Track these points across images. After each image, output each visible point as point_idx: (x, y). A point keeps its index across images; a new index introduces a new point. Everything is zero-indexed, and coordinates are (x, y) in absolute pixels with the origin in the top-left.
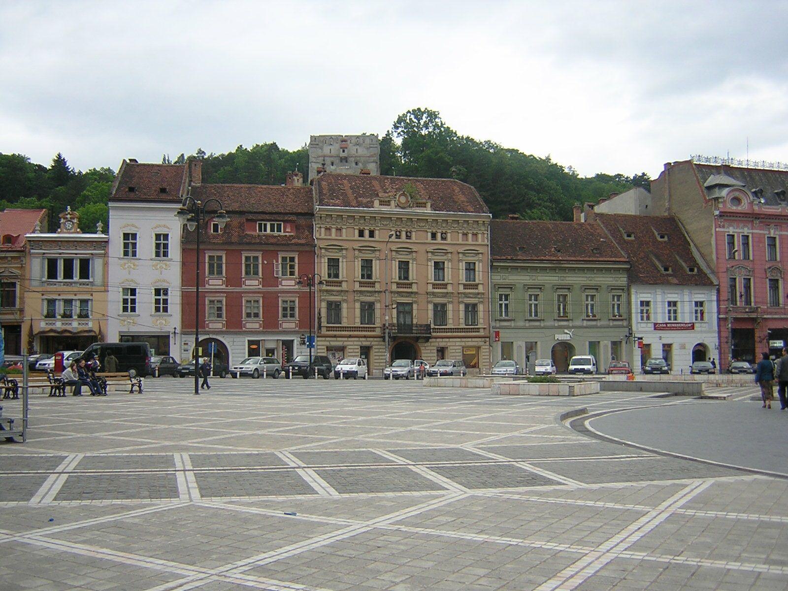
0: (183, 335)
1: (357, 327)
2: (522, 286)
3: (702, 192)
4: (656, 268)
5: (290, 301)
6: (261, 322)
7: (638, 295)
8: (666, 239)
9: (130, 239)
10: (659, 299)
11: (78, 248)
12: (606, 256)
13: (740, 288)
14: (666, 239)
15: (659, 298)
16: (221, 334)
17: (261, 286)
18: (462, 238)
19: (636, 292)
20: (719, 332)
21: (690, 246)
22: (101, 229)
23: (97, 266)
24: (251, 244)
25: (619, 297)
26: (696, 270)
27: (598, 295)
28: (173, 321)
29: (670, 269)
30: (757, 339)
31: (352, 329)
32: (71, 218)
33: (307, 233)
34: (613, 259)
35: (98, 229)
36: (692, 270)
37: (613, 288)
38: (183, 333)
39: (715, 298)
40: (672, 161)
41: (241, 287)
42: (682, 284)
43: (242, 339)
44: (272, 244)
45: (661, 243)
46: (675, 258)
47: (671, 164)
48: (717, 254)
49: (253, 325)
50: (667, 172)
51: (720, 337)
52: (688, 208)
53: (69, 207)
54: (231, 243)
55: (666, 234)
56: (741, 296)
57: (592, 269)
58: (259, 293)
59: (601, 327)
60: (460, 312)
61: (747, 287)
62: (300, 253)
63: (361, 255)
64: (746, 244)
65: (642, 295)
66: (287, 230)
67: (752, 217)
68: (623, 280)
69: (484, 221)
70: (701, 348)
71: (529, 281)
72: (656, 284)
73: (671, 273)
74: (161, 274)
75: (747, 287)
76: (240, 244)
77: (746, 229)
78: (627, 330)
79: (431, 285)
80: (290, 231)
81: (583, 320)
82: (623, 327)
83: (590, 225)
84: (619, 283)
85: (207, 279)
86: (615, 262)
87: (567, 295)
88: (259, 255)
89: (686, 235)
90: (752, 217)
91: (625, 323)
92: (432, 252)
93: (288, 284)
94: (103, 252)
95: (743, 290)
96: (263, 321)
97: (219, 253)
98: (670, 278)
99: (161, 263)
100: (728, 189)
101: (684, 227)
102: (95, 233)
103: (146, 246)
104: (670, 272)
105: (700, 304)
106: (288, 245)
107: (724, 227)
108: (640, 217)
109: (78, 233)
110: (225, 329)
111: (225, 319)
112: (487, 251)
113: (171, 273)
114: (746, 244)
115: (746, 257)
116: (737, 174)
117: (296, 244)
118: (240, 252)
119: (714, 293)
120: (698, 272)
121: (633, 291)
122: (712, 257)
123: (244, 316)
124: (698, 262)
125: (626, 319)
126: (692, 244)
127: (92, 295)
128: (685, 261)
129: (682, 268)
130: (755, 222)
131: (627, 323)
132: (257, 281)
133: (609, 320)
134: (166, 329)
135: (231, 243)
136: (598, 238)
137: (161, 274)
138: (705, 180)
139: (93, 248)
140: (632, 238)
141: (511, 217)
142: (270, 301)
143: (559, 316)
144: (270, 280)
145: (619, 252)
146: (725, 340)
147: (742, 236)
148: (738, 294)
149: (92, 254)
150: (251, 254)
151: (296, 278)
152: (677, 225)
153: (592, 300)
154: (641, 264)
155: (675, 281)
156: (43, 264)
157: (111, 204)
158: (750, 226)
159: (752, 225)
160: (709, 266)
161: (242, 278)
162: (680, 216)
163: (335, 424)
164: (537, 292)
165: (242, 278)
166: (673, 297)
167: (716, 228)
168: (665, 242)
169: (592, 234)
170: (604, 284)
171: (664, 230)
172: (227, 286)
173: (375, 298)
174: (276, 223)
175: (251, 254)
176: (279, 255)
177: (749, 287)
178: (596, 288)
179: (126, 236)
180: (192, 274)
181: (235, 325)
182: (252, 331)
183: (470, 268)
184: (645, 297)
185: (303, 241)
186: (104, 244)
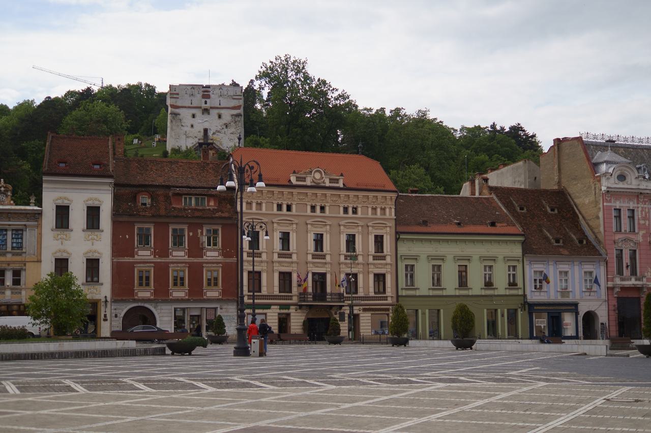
0: (113, 304)
1: (276, 296)
2: (426, 256)
5: (146, 271)
6: (187, 291)
8: (556, 211)
9: (63, 213)
11: (11, 219)
13: (626, 260)
15: (576, 268)
16: (150, 302)
17: (186, 257)
18: (246, 206)
21: (579, 218)
22: (34, 201)
23: (29, 237)
24: (180, 216)
28: (104, 290)
29: (561, 241)
31: (271, 297)
32: (4, 191)
33: (229, 206)
35: (31, 201)
36: (581, 242)
38: (115, 301)
40: (561, 137)
41: (169, 257)
43: (170, 307)
44: (197, 217)
45: (552, 214)
48: (604, 227)
49: (179, 293)
50: (556, 148)
52: (577, 182)
53: (2, 180)
54: (160, 216)
55: (556, 207)
56: (627, 266)
58: (151, 263)
60: (266, 285)
62: (224, 226)
63: (346, 230)
64: (632, 218)
66: (210, 204)
68: (517, 251)
69: (391, 197)
71: (406, 252)
73: (562, 244)
74: (93, 244)
76: (168, 217)
77: (631, 203)
79: (344, 256)
80: (213, 204)
85: (136, 250)
88: (185, 227)
92: (344, 226)
93: (212, 255)
94: (37, 223)
96: (189, 290)
97: (215, 227)
98: (561, 250)
99: (94, 234)
101: (573, 200)
102: (28, 204)
103: (78, 218)
104: (561, 244)
106: (212, 218)
107: (610, 201)
108: (532, 192)
109: (11, 205)
110: (153, 297)
111: (221, 288)
112: (392, 224)
113: (102, 245)
114: (632, 218)
116: (622, 150)
117: (221, 218)
118: (167, 224)
120: (587, 243)
122: (599, 230)
123: (170, 285)
124: (586, 234)
126: (580, 217)
127: (25, 265)
128: (574, 235)
129: (572, 240)
130: (640, 197)
132: (150, 251)
134: (97, 297)
135: (160, 216)
137: (93, 244)
139: (26, 220)
140: (525, 211)
141: (411, 191)
142: (196, 271)
143: (407, 286)
144: (196, 250)
146: (613, 308)
147: (614, 209)
148: (625, 265)
149: (25, 225)
150: (178, 227)
151: (220, 249)
153: (514, 270)
155: (566, 252)
157: (45, 178)
159: (638, 200)
161: (169, 249)
163: (62, 411)
165: (169, 249)
168: (555, 214)
172: (155, 257)
173: (358, 269)
174: (188, 197)
175: (178, 227)
176: (170, 227)
177: (635, 259)
179: (59, 208)
180: (120, 247)
181: (162, 295)
182: (178, 300)
183: (379, 240)
185: (226, 215)
186: (37, 216)
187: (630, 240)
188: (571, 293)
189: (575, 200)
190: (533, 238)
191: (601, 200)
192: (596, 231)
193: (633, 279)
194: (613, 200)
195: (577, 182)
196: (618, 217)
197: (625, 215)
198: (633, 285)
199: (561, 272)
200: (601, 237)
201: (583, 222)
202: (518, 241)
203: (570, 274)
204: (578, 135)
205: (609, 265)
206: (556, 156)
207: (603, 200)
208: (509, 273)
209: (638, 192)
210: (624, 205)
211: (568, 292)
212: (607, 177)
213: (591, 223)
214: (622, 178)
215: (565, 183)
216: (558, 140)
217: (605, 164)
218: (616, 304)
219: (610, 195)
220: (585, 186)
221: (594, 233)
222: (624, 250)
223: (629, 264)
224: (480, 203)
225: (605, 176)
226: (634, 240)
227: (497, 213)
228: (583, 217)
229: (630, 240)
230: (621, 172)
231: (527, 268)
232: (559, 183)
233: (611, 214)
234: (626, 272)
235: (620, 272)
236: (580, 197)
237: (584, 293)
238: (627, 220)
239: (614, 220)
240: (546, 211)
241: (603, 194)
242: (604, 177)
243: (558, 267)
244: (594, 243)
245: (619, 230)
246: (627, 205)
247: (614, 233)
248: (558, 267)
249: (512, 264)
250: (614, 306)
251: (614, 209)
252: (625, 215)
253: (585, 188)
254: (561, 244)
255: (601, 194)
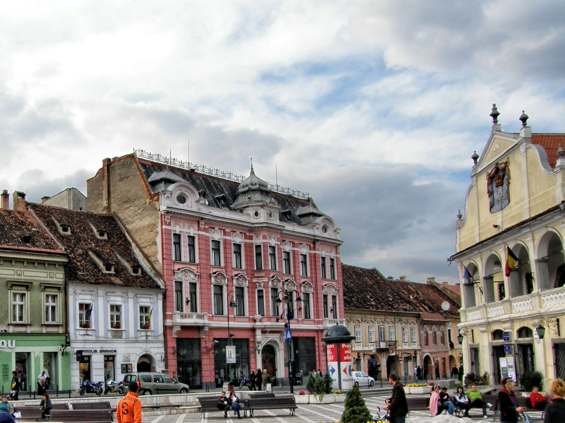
3: (146, 186)
4: (96, 266)
7: (78, 296)
8: (105, 237)
10: (101, 302)
12: (38, 247)
13: (186, 294)
14: (105, 237)
19: (75, 292)
20: (165, 342)
21: (131, 245)
25: (54, 297)
26: (140, 271)
27: (28, 294)
30: (204, 350)
34: (48, 250)
36: (135, 271)
37: (45, 286)
39: (160, 303)
40: (111, 157)
42: (126, 286)
46: (116, 257)
47: (110, 159)
51: (166, 347)
52: (129, 205)
55: (105, 231)
56: (187, 302)
57: (21, 261)
59: (32, 334)
61: (193, 293)
65: (142, 300)
67: (197, 219)
68: (58, 277)
70: (146, 360)
72: (99, 284)
75: (193, 293)
77: (192, 229)
78: (63, 338)
81: (9, 325)
82: (57, 334)
83: (19, 212)
84: (54, 280)
86: (50, 254)
87: (25, 294)
89: (127, 235)
90: (197, 219)
91: (61, 330)
95: (189, 296)
100: (174, 184)
101: (125, 227)
105: (144, 309)
107: (169, 224)
115: (192, 261)
119: (160, 297)
121: (71, 290)
125: (62, 325)
126: (133, 245)
131: (64, 329)
133: (42, 325)
136: (30, 227)
138: (148, 176)
140: (69, 233)
145: (54, 243)
147: (174, 234)
152: (116, 225)
154: (79, 261)
156: (488, 335)
158: (196, 227)
160: (153, 268)
162: (120, 215)
164: (22, 290)
166: (118, 301)
167: (162, 225)
168: (105, 240)
169: (23, 223)
170: (37, 281)
171: (103, 227)
177: (195, 293)
178: (27, 286)
184: (86, 299)
187: (191, 272)
188: (124, 333)
189: (127, 226)
190: (79, 264)
191: (160, 222)
192: (152, 259)
193: (194, 316)
194: (172, 223)
195: (129, 205)
196: (178, 244)
197: (185, 243)
198: (195, 323)
199: (112, 307)
200: (158, 267)
201: (136, 251)
202: (61, 264)
203: (123, 309)
204: (131, 152)
205: (168, 299)
206: (106, 178)
207: (162, 222)
208: (47, 304)
209: (199, 217)
210: (186, 230)
211: (120, 331)
212: (166, 195)
213: (146, 251)
214: (182, 199)
215: (114, 208)
216: (108, 160)
217: (163, 183)
218: (175, 346)
219: (169, 217)
220: (140, 209)
221: (149, 262)
222: (184, 283)
223: (189, 299)
224: (12, 217)
225: (165, 194)
226: (195, 272)
227: (33, 229)
228: (137, 245)
229: (191, 272)
230: (181, 193)
231: (71, 298)
232: (108, 208)
233: (171, 240)
234: (187, 309)
235: (180, 308)
236: (133, 222)
237: (139, 332)
238: (187, 249)
239: (173, 247)
240: (94, 236)
241: (162, 215)
242: (163, 195)
243: (138, 300)
244: (152, 274)
245: (178, 259)
246: (188, 231)
247: (174, 262)
248: (138, 300)
249: (51, 293)
250: (173, 348)
251: (174, 234)
252: (185, 243)
253: (140, 211)
254: (112, 272)
255: (160, 215)
